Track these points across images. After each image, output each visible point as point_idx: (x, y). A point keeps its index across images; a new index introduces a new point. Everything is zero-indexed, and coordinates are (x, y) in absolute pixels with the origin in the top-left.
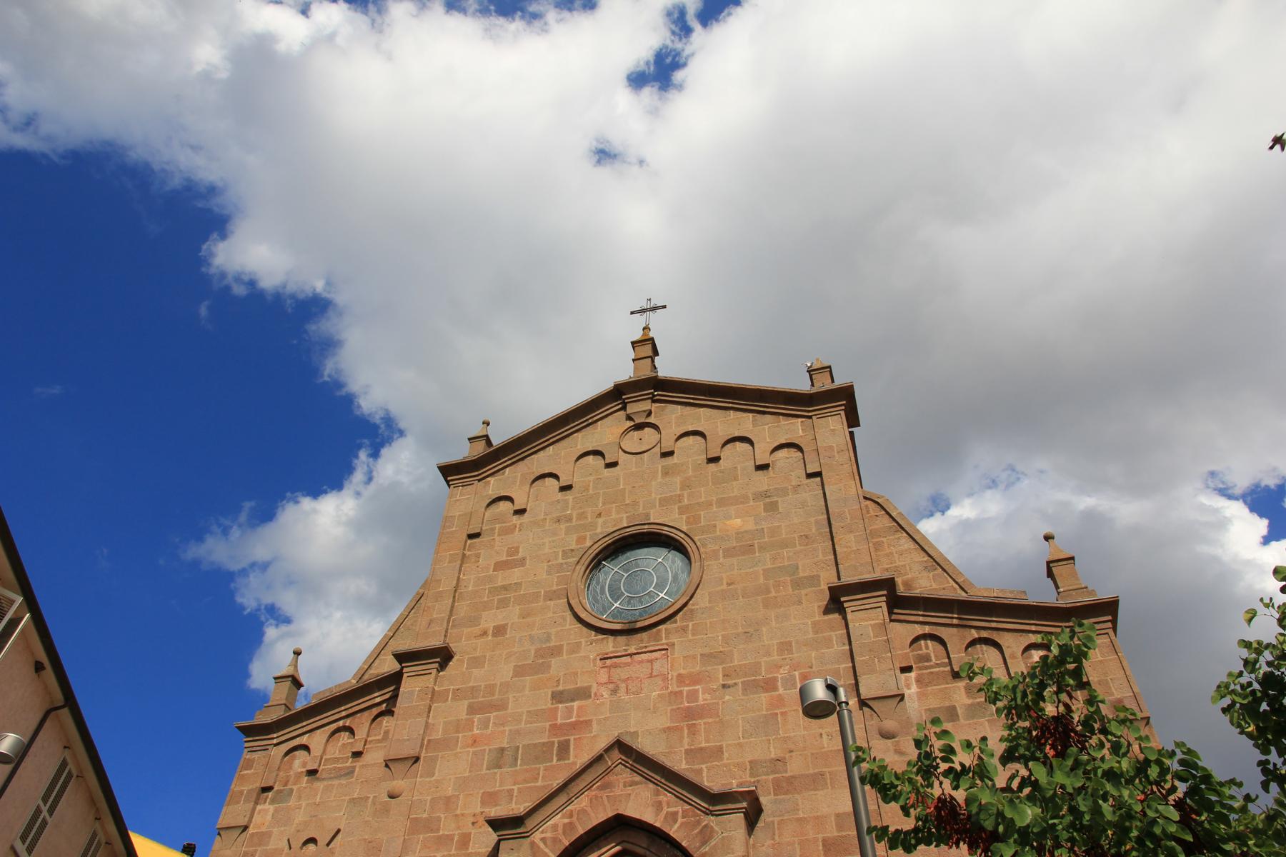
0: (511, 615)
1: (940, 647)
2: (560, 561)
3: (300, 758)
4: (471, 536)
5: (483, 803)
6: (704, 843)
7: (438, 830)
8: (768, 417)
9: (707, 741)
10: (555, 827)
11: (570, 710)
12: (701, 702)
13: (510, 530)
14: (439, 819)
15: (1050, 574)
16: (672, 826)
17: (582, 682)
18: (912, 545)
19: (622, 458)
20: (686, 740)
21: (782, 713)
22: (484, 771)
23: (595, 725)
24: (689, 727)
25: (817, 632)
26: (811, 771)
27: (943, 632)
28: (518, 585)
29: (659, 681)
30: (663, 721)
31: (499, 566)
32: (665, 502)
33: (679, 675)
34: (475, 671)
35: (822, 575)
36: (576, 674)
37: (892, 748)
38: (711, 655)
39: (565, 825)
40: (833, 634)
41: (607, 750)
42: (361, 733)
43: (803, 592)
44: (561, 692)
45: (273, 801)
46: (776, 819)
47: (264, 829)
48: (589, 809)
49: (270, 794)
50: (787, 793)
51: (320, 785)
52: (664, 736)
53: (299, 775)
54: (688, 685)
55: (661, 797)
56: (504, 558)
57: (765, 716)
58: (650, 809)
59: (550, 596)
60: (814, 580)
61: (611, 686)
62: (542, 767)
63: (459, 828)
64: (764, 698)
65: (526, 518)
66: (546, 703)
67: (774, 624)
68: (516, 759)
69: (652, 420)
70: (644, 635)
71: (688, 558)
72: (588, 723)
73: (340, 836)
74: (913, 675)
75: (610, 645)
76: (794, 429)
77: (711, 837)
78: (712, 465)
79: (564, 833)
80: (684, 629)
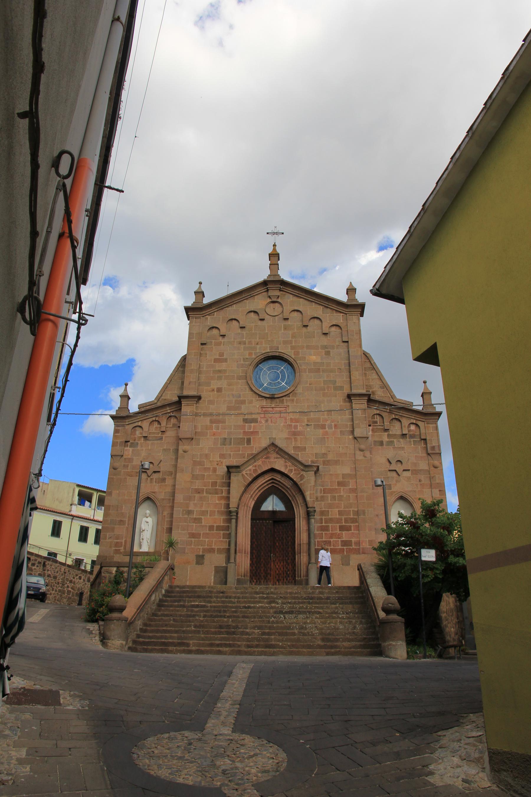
0: (223, 384)
1: (381, 419)
2: (242, 362)
3: (138, 432)
4: (202, 344)
5: (220, 457)
6: (301, 480)
7: (204, 465)
8: (329, 310)
10: (250, 470)
11: (250, 427)
13: (219, 344)
14: (204, 462)
15: (422, 396)
18: (376, 377)
19: (267, 317)
20: (293, 443)
23: (260, 434)
24: (295, 438)
28: (225, 371)
30: (285, 435)
31: (216, 360)
32: (285, 342)
33: (291, 419)
34: (211, 406)
35: (345, 386)
41: (269, 446)
42: (164, 423)
43: (338, 392)
44: (247, 419)
45: (131, 446)
47: (129, 457)
49: (129, 443)
50: (327, 465)
51: (150, 442)
55: (287, 464)
56: (218, 357)
59: (239, 378)
60: (341, 388)
65: (226, 340)
66: (241, 423)
69: (279, 300)
70: (278, 400)
71: (294, 370)
72: (257, 432)
74: (371, 428)
75: (264, 403)
76: (339, 319)
77: (304, 478)
78: (304, 329)
80: (293, 400)
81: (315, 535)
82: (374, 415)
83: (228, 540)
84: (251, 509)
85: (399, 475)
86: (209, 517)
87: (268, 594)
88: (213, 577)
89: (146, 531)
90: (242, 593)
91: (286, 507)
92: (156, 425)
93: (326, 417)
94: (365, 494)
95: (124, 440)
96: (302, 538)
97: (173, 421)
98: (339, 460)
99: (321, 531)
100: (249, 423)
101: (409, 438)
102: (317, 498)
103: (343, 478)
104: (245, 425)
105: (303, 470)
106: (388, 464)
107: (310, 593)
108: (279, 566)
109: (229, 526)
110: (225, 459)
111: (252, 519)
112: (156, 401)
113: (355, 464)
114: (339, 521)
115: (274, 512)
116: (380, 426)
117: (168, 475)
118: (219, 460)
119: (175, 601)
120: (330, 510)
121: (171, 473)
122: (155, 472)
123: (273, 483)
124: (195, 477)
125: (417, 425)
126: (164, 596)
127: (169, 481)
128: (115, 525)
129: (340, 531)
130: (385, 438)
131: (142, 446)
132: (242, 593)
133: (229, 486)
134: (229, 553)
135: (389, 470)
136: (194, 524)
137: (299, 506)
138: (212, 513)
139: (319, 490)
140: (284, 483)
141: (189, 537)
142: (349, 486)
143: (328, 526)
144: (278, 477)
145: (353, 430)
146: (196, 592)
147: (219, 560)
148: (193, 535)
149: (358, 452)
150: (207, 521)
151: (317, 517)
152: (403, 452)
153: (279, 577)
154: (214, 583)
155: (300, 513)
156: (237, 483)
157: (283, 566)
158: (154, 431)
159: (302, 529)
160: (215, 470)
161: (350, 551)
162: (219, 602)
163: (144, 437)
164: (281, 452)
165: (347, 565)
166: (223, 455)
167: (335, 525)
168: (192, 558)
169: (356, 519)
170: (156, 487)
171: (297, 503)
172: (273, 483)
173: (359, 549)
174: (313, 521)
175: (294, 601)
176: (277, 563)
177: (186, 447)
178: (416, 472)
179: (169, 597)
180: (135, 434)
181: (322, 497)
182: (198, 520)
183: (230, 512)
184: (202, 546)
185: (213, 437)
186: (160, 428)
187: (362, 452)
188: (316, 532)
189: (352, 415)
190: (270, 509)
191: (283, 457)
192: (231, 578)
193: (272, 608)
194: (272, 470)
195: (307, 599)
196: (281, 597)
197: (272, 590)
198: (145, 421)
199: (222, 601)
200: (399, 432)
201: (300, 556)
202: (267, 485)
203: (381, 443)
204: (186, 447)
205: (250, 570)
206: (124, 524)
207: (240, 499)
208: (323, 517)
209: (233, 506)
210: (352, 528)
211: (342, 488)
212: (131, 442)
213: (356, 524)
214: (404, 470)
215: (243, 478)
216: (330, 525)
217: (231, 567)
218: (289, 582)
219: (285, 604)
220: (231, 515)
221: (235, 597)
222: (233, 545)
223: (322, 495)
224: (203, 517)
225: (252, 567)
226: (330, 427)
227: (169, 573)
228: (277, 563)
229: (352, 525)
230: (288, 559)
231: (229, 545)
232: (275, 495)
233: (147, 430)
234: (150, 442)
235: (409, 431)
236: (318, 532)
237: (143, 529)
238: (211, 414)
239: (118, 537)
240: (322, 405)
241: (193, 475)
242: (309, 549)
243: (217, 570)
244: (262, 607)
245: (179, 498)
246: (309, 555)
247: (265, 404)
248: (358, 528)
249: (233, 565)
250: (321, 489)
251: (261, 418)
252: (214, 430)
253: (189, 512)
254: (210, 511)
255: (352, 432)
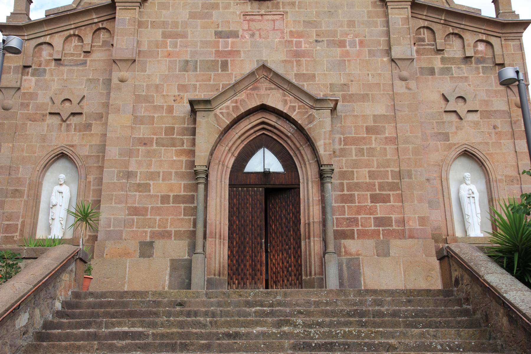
3: (46, 52)
5: (179, 90)
6: (310, 123)
7: (153, 102)
9: (307, 70)
10: (228, 107)
11: (227, 44)
12: (303, 48)
14: (153, 96)
16: (292, 113)
17: (233, 27)
20: (295, 69)
21: (348, 60)
22: (177, 73)
23: (242, 53)
24: (298, 61)
25: (369, 18)
26: (362, 93)
27: (435, 27)
29: (278, 33)
30: (282, 56)
33: (291, 31)
34: (164, 12)
36: (228, 22)
37: (405, 86)
38: (309, 22)
39: (233, 106)
40: (379, 20)
41: (258, 69)
42: (88, 40)
44: (221, 32)
45: (33, 75)
46: (343, 114)
47: (31, 91)
48: (246, 100)
49: (30, 70)
52: (283, 64)
53: (48, 62)
54: (296, 38)
55: (286, 98)
57: (339, 61)
58: (281, 103)
61: (250, 32)
62: (212, 74)
63: (166, 102)
64: (339, 50)
67: (345, 9)
68: (196, 68)
72: (238, 52)
73: (85, 100)
77: (313, 120)
79: (233, 111)
81: (333, 208)
82: (420, 28)
83: (192, 218)
84: (229, 170)
85: (461, 119)
86: (161, 182)
87: (272, 305)
88: (167, 277)
89: (58, 206)
90: (219, 304)
91: (284, 166)
92: (75, 42)
93: (346, 29)
94: (411, 146)
95: (21, 64)
96: (311, 213)
97: (103, 35)
98: (367, 95)
99: (342, 202)
100: (224, 38)
101: (476, 63)
102: (334, 152)
103: (375, 121)
104: (218, 42)
105: (312, 107)
106: (443, 102)
107: (355, 304)
108: (276, 260)
109: (193, 196)
110: (187, 92)
111: (231, 185)
112: (75, 6)
113: (394, 100)
114: (369, 187)
115: (266, 174)
116: (428, 45)
117: (95, 120)
118: (177, 93)
119: (78, 326)
120: (355, 170)
121: (100, 116)
122: (73, 114)
123: (263, 129)
124: (137, 120)
125: (488, 43)
126: (59, 314)
127: (96, 129)
128: (6, 197)
129: (372, 202)
130: (437, 62)
131: (52, 75)
132: (219, 304)
133: (194, 133)
134: (194, 238)
135: (445, 112)
136: (137, 193)
137: (305, 164)
138: (167, 176)
139: (337, 140)
140: (282, 129)
141: (129, 214)
142: (385, 133)
143: (352, 196)
144: (272, 119)
145: (390, 48)
146: (125, 305)
147: (178, 249)
148: (135, 211)
149: (398, 83)
150: (158, 188)
151: (336, 181)
152: (466, 84)
153: (276, 277)
154: (170, 287)
155: (307, 176)
156: (207, 127)
157: (282, 259)
158: (72, 51)
159: (311, 199)
160: (170, 109)
161: (390, 234)
162: (171, 325)
163: (56, 60)
164: (277, 80)
165: (386, 256)
166: (183, 86)
167: (363, 193)
168: (133, 246)
169: (398, 184)
170: (76, 138)
171: (304, 160)
172: (263, 129)
173: (403, 231)
174: (329, 186)
175: (327, 319)
176: (274, 256)
177: (124, 74)
178: (487, 114)
179: (67, 316)
180: (41, 56)
181: (342, 150)
182: (143, 187)
183: (196, 173)
184: (149, 227)
185: (168, 59)
186: (82, 46)
187: (404, 82)
188: (334, 204)
189: (388, 26)
190: (259, 169)
191: (280, 87)
192: (198, 278)
193: (285, 335)
194: (263, 108)
195: (353, 316)
196: (300, 312)
197: (278, 298)
198: (57, 35)
199: (179, 322)
200: (459, 55)
201: (309, 242)
202: (255, 132)
203: (432, 71)
204: (124, 74)
205: (229, 265)
206: (21, 196)
207: (211, 154)
208: (345, 182)
209: (200, 161)
210: (392, 198)
211: (374, 137)
212: (33, 67)
213: (398, 192)
214: (469, 111)
215: (217, 120)
216: (356, 193)
217: (198, 262)
218: (291, 284)
219: (310, 326)
220: (198, 177)
221: (206, 314)
222: (200, 225)
223: (342, 146)
224: (151, 183)
225: (232, 261)
226: (353, 44)
227: (73, 266)
228: (274, 256)
229: (391, 193)
230: (290, 248)
231: (195, 225)
232: (267, 148)
233: (61, 49)
234: (65, 69)
235: (475, 53)
236: (336, 205)
237: (54, 203)
238: (164, 24)
239: (10, 217)
240: (340, 11)
241: (136, 117)
242: (324, 232)
243: (175, 265)
244: (263, 334)
245: (113, 152)
246: (325, 241)
247: (250, 10)
248: (401, 198)
249: (201, 256)
250: (340, 138)
251: (243, 30)
252: (169, 49)
253: (129, 175)
254: (163, 172)
255: (388, 52)
